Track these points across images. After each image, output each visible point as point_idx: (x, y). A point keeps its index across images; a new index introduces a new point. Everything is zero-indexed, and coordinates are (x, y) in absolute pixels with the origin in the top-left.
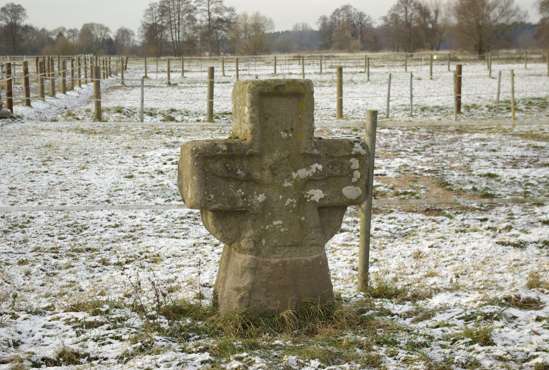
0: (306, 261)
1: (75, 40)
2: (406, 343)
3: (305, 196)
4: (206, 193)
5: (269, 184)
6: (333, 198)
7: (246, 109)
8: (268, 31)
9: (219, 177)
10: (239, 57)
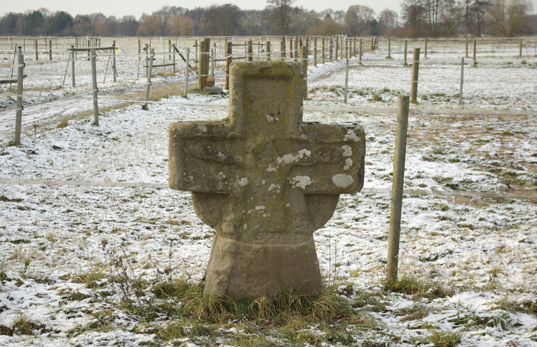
0: (290, 249)
1: (342, 21)
2: (362, 342)
3: (291, 182)
4: (185, 174)
5: (251, 168)
6: (321, 185)
8: (529, 13)
9: (199, 158)
10: (407, 39)
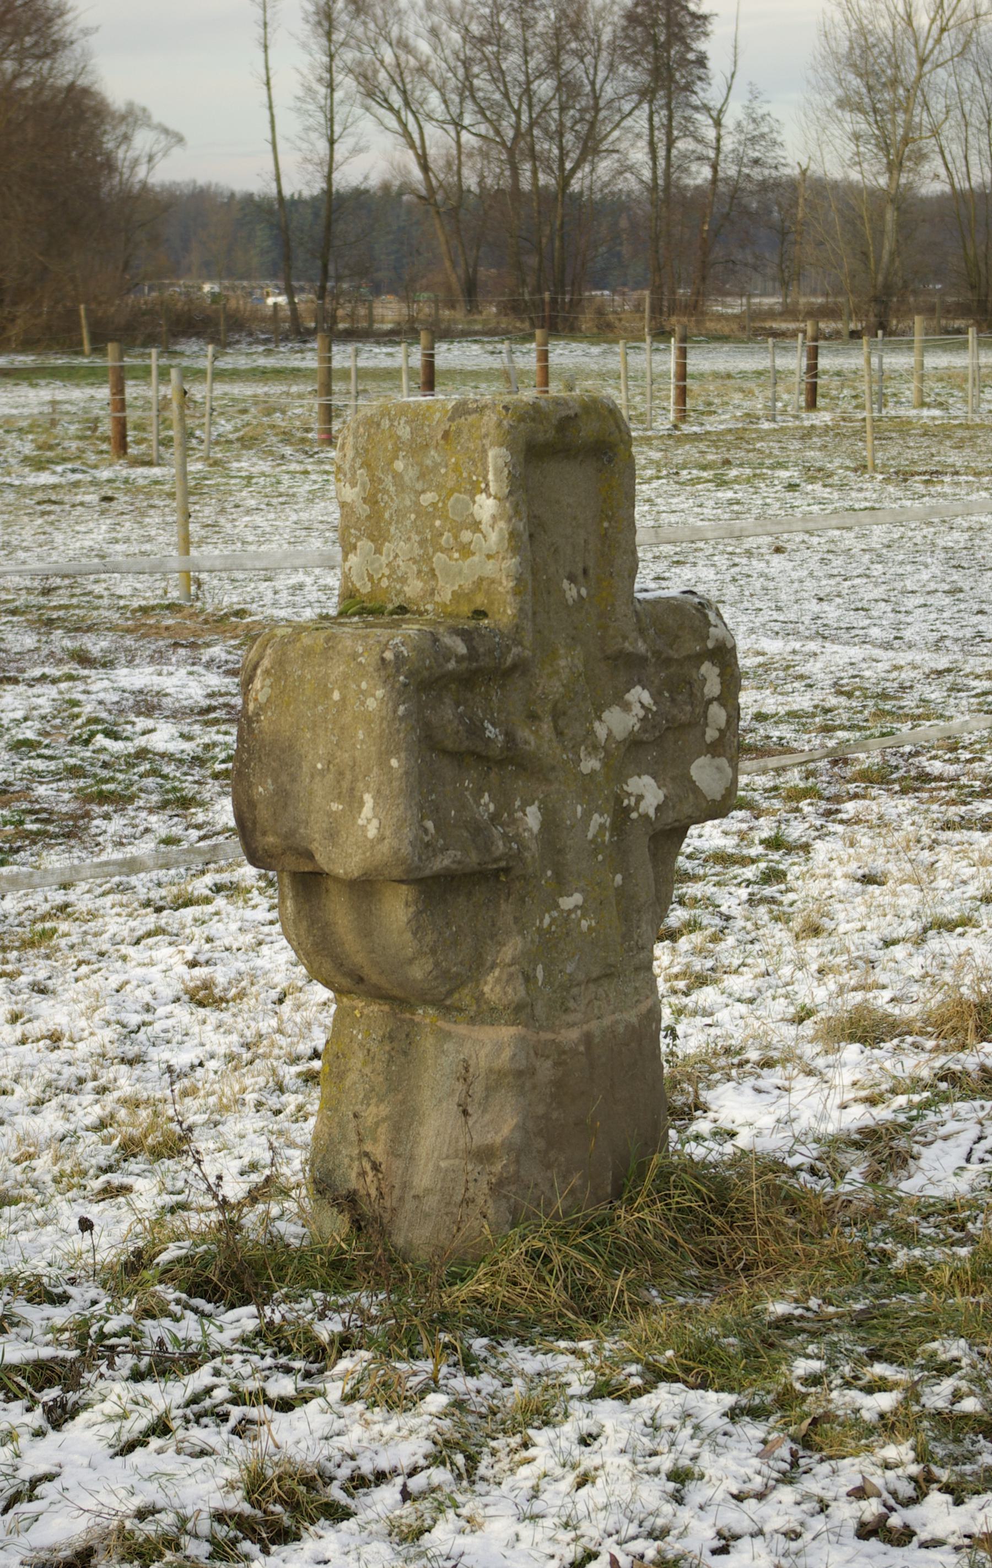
3: (626, 802)
7: (486, 507)
9: (445, 752)
